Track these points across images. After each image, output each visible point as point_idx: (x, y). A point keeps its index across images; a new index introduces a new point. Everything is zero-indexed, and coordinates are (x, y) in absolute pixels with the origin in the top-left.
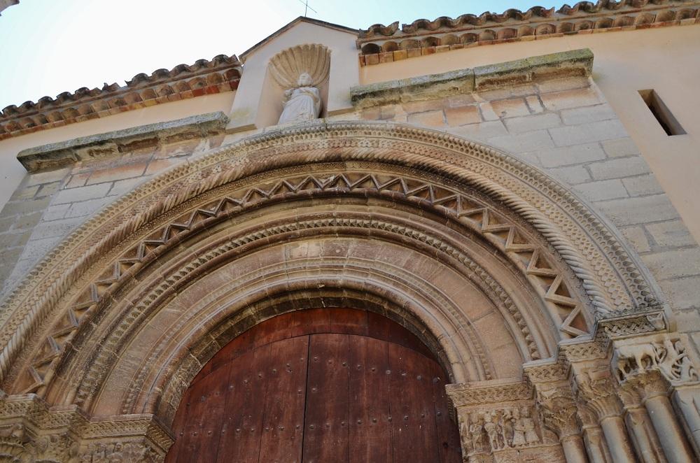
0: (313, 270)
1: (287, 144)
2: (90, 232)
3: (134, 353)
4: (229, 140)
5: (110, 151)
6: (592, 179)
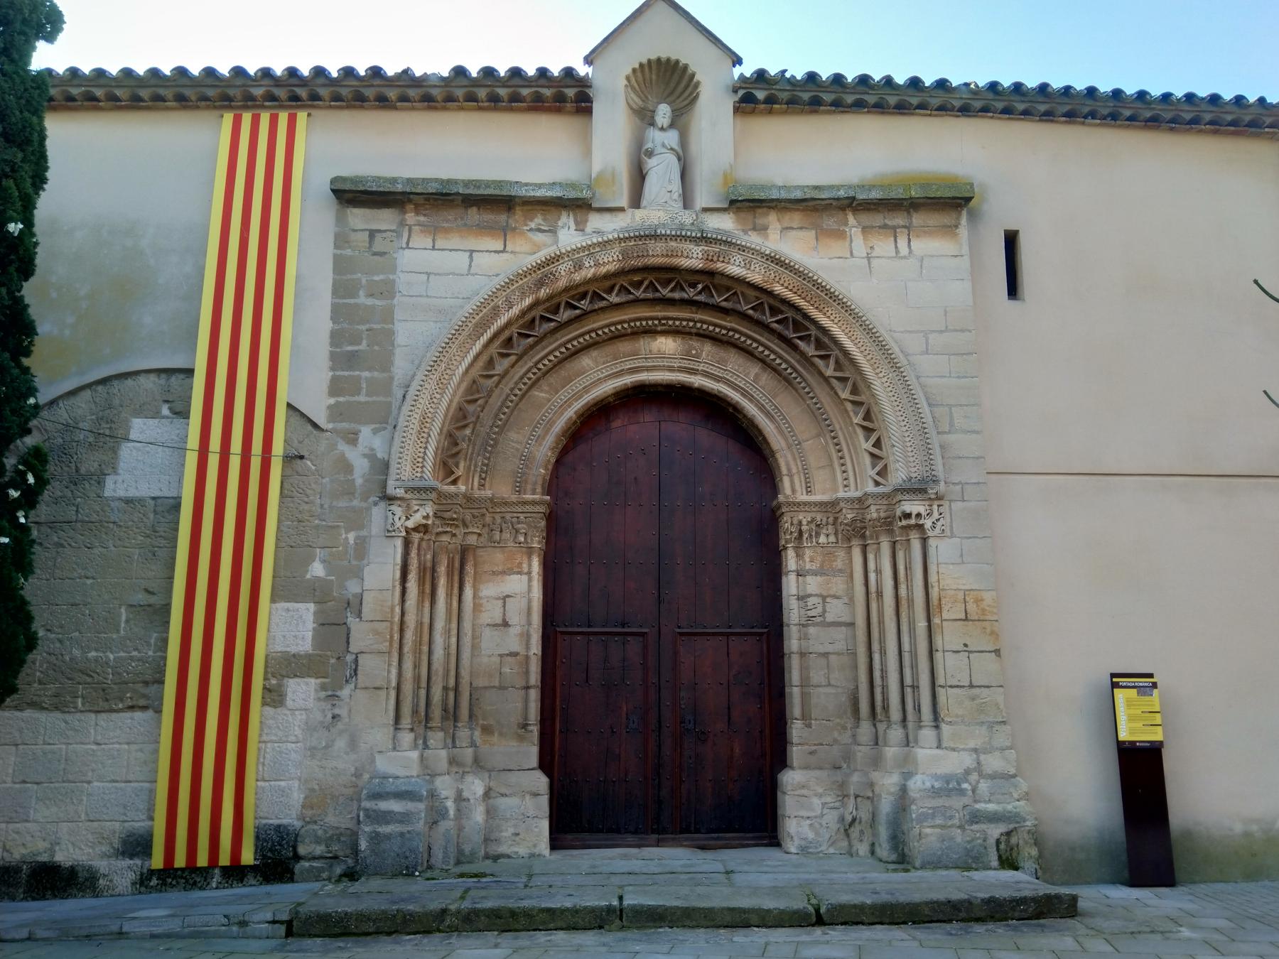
0: (671, 369)
3: (513, 435)
6: (927, 353)
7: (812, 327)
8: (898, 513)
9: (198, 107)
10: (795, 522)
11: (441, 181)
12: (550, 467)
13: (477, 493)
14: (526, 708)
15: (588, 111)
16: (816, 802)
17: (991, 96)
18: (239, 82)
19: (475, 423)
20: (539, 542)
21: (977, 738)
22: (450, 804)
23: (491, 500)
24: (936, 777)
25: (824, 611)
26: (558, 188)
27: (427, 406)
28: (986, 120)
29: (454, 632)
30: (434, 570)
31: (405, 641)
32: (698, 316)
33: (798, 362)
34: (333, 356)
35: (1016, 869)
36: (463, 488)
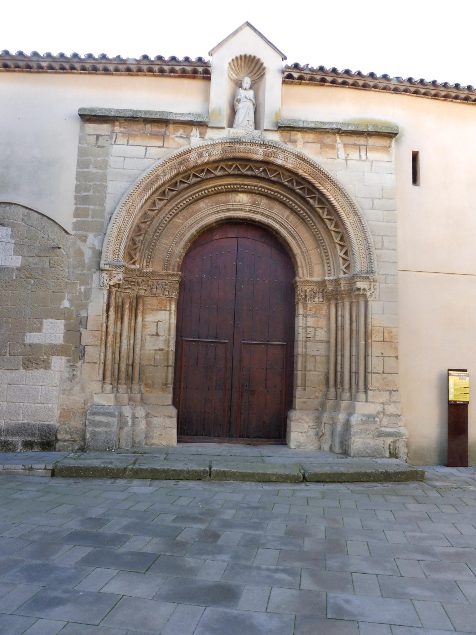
0: (245, 211)
1: (242, 146)
2: (144, 184)
3: (164, 241)
4: (213, 136)
5: (138, 121)
6: (372, 208)
7: (317, 193)
8: (354, 288)
9: (14, 71)
10: (304, 290)
11: (133, 111)
12: (182, 258)
13: (145, 269)
14: (167, 376)
15: (208, 79)
16: (306, 425)
17: (408, 84)
18: (35, 59)
19: (145, 234)
20: (175, 295)
21: (385, 397)
22: (130, 421)
23: (152, 273)
24: (364, 415)
25: (315, 335)
26: (192, 116)
27: (121, 224)
28: (406, 96)
29: (132, 337)
30: (123, 307)
31: (108, 341)
32: (260, 184)
33: (309, 210)
34: (76, 197)
35: (397, 458)
36: (138, 266)
